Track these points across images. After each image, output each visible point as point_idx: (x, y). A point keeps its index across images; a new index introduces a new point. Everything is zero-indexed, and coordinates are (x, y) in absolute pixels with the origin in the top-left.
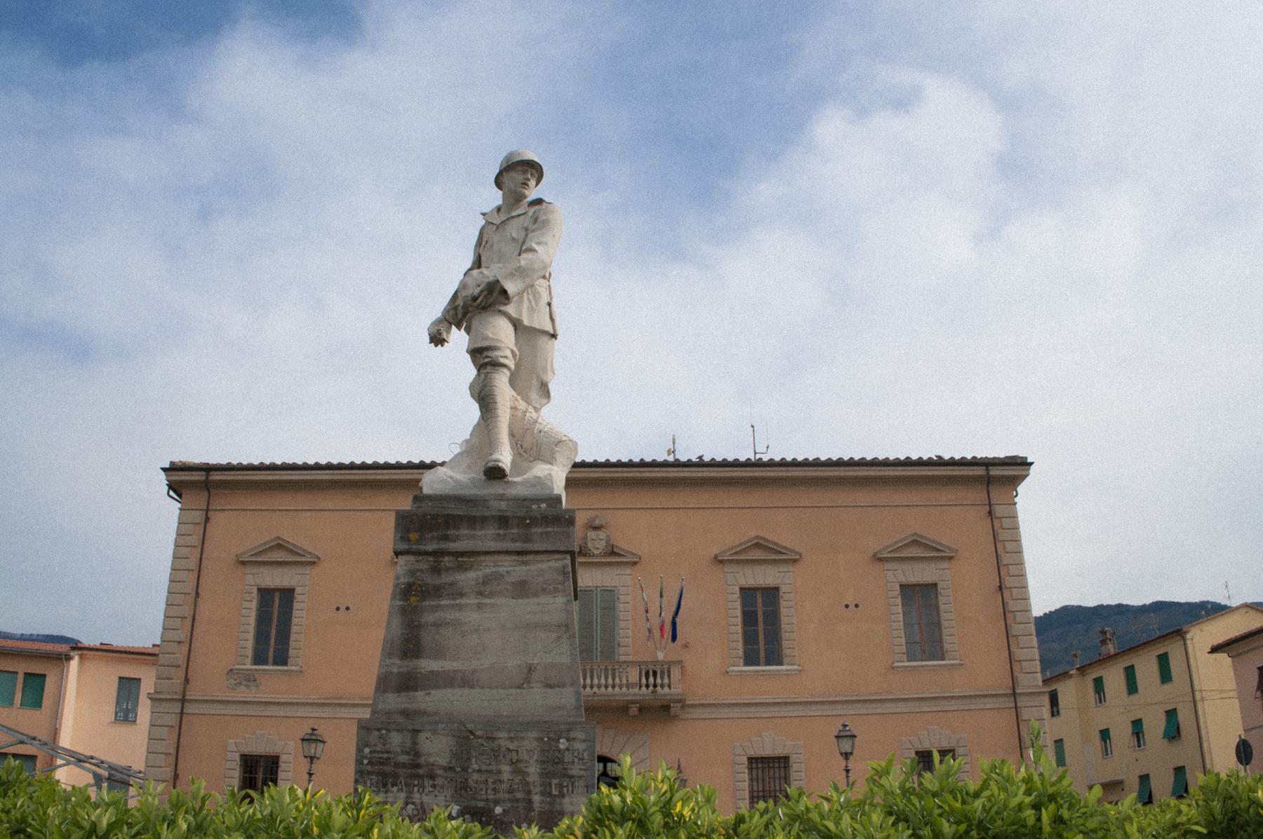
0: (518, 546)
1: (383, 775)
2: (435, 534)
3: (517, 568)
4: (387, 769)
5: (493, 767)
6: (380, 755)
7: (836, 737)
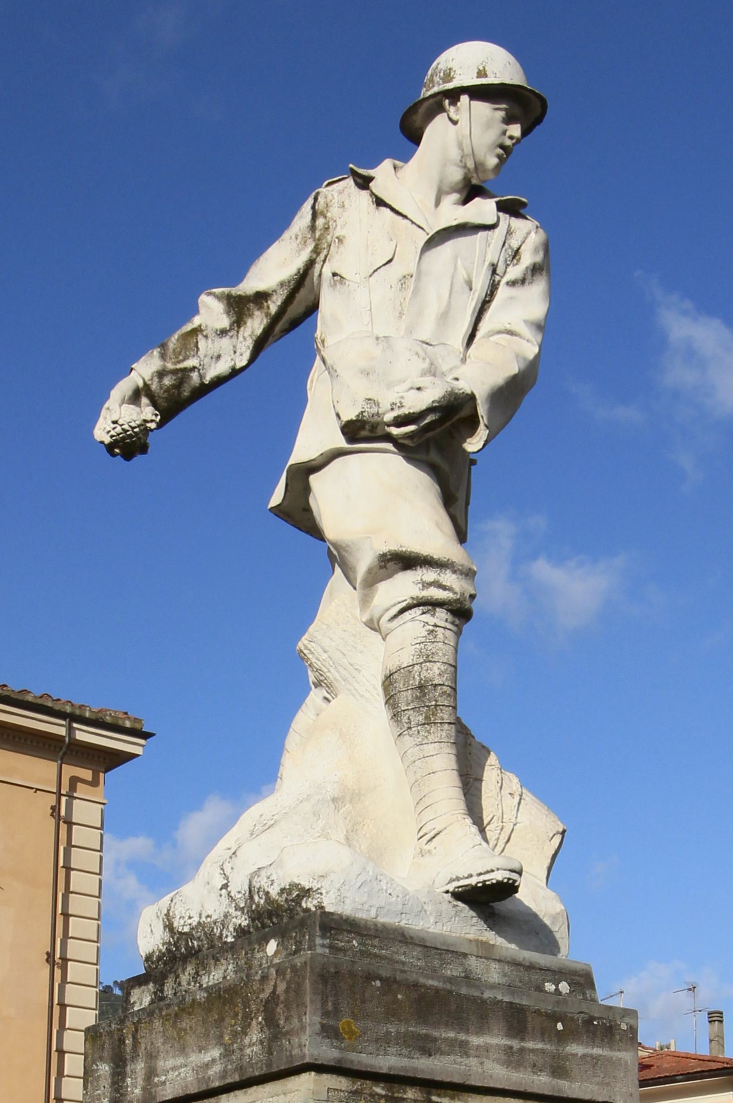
2: (393, 1029)
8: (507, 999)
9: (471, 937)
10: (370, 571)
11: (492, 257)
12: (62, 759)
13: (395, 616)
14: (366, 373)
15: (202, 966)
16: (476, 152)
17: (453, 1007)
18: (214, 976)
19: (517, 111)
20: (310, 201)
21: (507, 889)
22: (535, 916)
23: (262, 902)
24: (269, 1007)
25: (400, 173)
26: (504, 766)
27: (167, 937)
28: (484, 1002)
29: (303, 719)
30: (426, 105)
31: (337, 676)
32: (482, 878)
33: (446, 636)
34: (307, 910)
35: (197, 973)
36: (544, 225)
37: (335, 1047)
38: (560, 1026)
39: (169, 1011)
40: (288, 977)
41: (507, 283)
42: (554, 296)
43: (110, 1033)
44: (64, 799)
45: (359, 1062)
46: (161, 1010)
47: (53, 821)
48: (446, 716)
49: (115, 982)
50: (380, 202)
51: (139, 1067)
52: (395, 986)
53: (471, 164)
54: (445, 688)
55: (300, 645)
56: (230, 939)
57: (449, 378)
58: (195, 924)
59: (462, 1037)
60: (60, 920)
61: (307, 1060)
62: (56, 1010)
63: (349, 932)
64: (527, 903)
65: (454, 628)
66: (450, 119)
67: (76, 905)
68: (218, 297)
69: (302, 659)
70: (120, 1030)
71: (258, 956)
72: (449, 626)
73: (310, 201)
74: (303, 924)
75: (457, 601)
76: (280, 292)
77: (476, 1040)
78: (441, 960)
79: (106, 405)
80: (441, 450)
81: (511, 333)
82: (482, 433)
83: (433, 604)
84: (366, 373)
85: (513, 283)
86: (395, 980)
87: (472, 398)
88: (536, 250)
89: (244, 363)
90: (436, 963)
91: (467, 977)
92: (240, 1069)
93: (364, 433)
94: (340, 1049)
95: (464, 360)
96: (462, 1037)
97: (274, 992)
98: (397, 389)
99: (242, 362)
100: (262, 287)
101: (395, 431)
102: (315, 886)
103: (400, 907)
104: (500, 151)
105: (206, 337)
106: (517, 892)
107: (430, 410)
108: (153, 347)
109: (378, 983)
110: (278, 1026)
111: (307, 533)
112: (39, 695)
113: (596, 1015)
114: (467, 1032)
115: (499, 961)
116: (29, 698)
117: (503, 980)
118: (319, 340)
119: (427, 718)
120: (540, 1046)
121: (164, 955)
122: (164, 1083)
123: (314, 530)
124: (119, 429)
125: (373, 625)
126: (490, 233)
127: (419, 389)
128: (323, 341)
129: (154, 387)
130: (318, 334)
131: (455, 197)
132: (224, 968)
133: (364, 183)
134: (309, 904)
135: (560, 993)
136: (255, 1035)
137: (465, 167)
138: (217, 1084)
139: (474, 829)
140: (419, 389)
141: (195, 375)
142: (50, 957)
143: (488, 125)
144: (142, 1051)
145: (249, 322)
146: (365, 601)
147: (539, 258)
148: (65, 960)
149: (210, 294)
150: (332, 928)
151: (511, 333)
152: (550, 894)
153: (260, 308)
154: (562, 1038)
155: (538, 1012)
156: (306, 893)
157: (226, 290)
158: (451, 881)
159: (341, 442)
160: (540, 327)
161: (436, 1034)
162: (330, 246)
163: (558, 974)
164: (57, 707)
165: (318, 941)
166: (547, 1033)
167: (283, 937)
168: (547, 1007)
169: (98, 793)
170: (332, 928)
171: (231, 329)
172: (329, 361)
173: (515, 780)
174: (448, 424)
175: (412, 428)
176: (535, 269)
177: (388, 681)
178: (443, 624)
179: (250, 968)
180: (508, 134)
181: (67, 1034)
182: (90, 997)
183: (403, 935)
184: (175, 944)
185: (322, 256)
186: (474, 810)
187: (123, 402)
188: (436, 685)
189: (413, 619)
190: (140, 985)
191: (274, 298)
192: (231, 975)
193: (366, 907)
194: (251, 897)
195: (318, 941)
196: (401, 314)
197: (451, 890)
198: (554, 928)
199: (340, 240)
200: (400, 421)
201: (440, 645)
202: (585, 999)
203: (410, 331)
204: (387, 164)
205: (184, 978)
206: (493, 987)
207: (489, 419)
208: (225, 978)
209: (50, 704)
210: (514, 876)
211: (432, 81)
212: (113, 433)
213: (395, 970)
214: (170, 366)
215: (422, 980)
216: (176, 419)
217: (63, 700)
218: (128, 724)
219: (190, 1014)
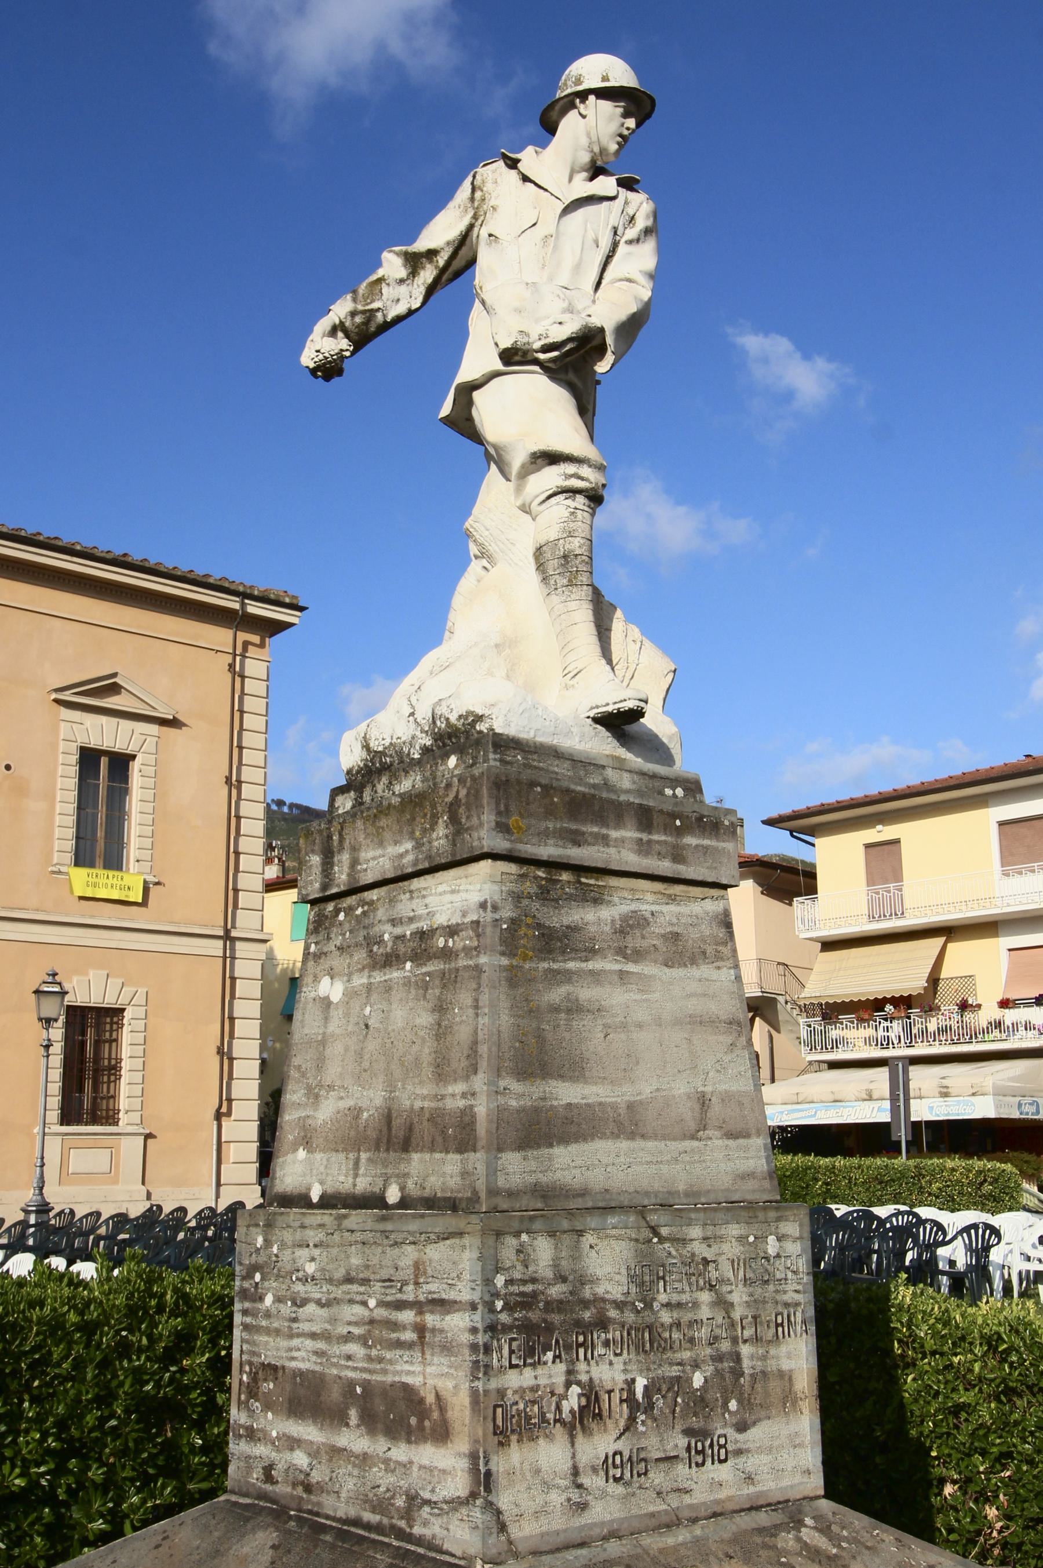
0: (665, 867)
1: (527, 1328)
2: (551, 825)
3: (665, 909)
4: (534, 1316)
5: (685, 1298)
6: (522, 1289)
7: (37, 992)
8: (637, 801)
9: (607, 752)
10: (523, 466)
11: (614, 220)
12: (237, 627)
13: (544, 501)
14: (519, 311)
15: (394, 777)
16: (601, 139)
17: (597, 808)
18: (405, 785)
19: (633, 108)
20: (470, 178)
21: (636, 714)
22: (656, 736)
23: (443, 726)
24: (453, 809)
25: (541, 156)
26: (629, 619)
27: (364, 755)
28: (620, 804)
29: (466, 584)
30: (561, 103)
31: (496, 548)
32: (617, 706)
33: (583, 516)
34: (480, 732)
35: (390, 783)
36: (652, 197)
37: (507, 840)
38: (678, 823)
39: (370, 813)
40: (468, 784)
41: (626, 242)
42: (661, 251)
43: (320, 832)
44: (238, 658)
45: (526, 852)
46: (362, 812)
47: (230, 675)
48: (584, 579)
49: (273, 800)
50: (526, 179)
51: (345, 857)
52: (552, 791)
53: (596, 150)
54: (584, 558)
55: (467, 525)
56: (417, 756)
57: (583, 315)
58: (387, 744)
59: (604, 831)
60: (236, 751)
61: (485, 850)
62: (233, 820)
63: (515, 749)
64: (649, 726)
65: (590, 511)
66: (580, 114)
67: (248, 739)
68: (397, 254)
69: (468, 536)
70: (329, 829)
71: (441, 768)
72: (586, 509)
73: (470, 178)
74: (478, 743)
75: (592, 489)
76: (447, 249)
77: (614, 834)
78: (586, 771)
79: (311, 338)
80: (577, 371)
81: (629, 280)
82: (609, 358)
83: (574, 492)
84: (519, 311)
85: (630, 242)
86: (552, 787)
87: (602, 330)
88: (647, 217)
89: (418, 305)
90: (582, 773)
91: (605, 784)
92: (429, 857)
93: (517, 358)
94: (511, 841)
95: (594, 302)
96: (604, 831)
97: (457, 797)
98: (543, 323)
99: (416, 305)
100: (432, 245)
101: (542, 356)
102: (487, 712)
103: (552, 729)
104: (620, 139)
105: (388, 285)
106: (643, 716)
107: (569, 340)
108: (346, 293)
109: (539, 789)
110: (461, 823)
111: (468, 438)
112: (218, 577)
113: (706, 813)
114: (608, 827)
115: (630, 771)
116: (211, 581)
117: (633, 787)
118: (477, 287)
119: (570, 581)
120: (663, 838)
121: (362, 769)
122: (366, 870)
123: (475, 436)
124: (321, 357)
125: (525, 509)
126: (611, 203)
127: (560, 323)
128: (481, 288)
129: (348, 324)
130: (476, 282)
131: (585, 175)
132: (413, 778)
133: (513, 164)
134: (482, 727)
135: (677, 797)
136: (441, 831)
137: (592, 151)
138: (410, 870)
139: (608, 668)
140: (560, 323)
141: (379, 315)
142: (228, 780)
143: (611, 119)
144: (347, 844)
145: (422, 273)
146: (519, 490)
147: (650, 223)
148: (239, 782)
149: (391, 251)
150: (501, 746)
151: (629, 280)
152: (667, 719)
153: (431, 261)
154: (679, 832)
155: (661, 811)
156: (480, 718)
157: (404, 248)
158: (592, 708)
159: (499, 366)
160: (652, 276)
161: (584, 829)
162: (485, 213)
163: (675, 782)
164: (233, 587)
165: (491, 756)
166: (668, 828)
167: (462, 753)
168: (668, 807)
169: (264, 654)
170: (501, 746)
171: (408, 279)
172: (488, 302)
173: (636, 630)
174: (582, 351)
175: (555, 354)
176: (647, 231)
177: (539, 552)
178: (582, 507)
179: (434, 778)
180: (626, 125)
181: (242, 839)
182: (259, 811)
183: (556, 751)
184: (371, 761)
185: (480, 221)
186: (606, 653)
187: (324, 336)
188: (576, 555)
189: (558, 504)
190: (343, 793)
191: (442, 254)
192: (419, 785)
193: (527, 729)
194: (434, 722)
195: (491, 756)
196: (544, 266)
197: (592, 715)
198: (671, 746)
199: (494, 208)
200: (546, 349)
201: (580, 523)
202: (696, 801)
203: (551, 279)
204: (530, 150)
205: (380, 787)
206: (628, 792)
207: (615, 347)
208: (413, 786)
209: (227, 585)
210: (642, 704)
211: (565, 84)
212: (316, 359)
213: (552, 778)
214: (360, 307)
215: (573, 787)
216: (368, 346)
217: (238, 582)
218: (287, 600)
219: (386, 815)
